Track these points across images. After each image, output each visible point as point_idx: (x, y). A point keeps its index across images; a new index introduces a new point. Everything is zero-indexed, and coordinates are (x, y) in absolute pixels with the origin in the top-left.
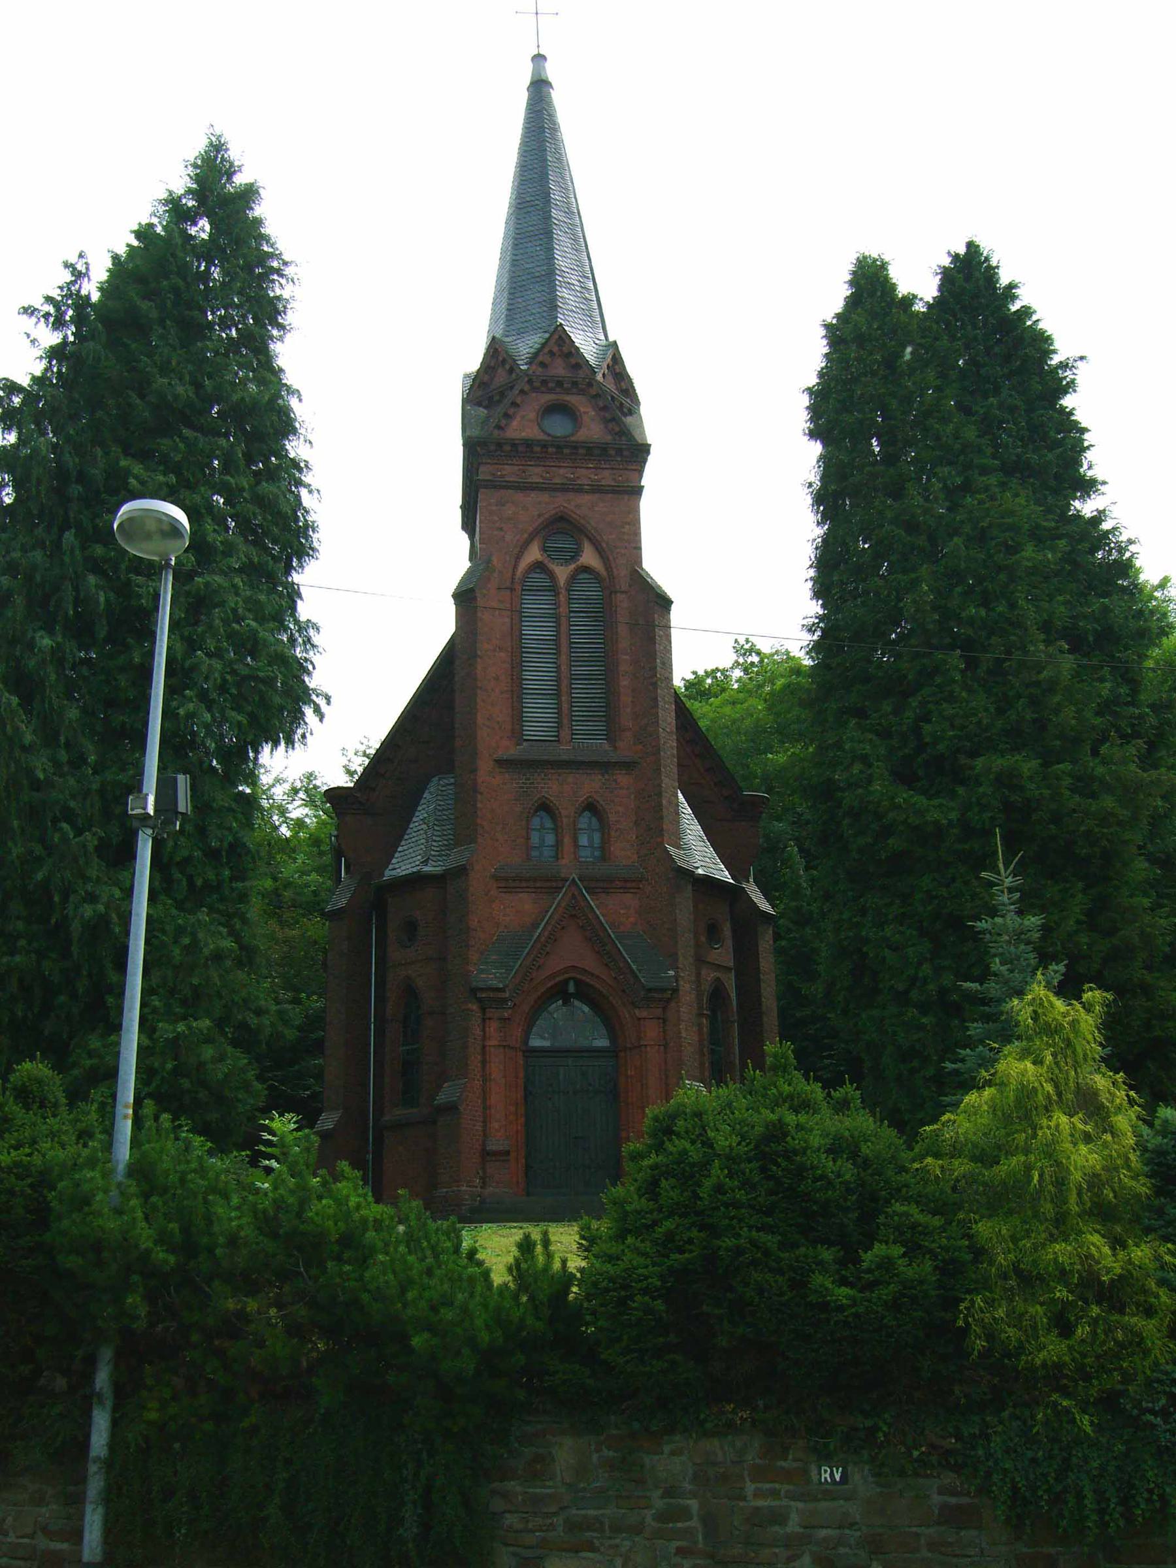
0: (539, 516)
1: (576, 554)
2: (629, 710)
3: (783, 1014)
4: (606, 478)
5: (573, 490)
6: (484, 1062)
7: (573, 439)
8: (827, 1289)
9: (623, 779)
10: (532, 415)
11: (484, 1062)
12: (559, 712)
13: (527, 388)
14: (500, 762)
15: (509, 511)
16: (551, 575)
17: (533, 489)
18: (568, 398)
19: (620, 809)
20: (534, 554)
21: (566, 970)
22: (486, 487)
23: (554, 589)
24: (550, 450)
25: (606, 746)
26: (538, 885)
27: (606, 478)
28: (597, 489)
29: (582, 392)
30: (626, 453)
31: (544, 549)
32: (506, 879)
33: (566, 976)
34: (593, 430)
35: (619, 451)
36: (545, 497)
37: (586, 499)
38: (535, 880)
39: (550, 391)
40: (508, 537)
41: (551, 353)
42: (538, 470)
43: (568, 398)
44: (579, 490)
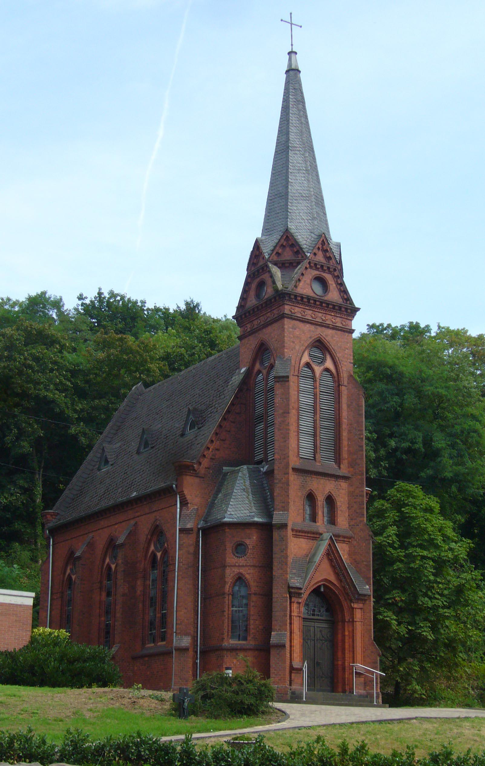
0: (310, 338)
1: (323, 361)
2: (346, 449)
3: (165, 578)
4: (338, 322)
5: (325, 327)
6: (291, 624)
7: (323, 298)
8: (163, 705)
9: (344, 484)
10: (308, 281)
11: (291, 624)
12: (315, 445)
13: (308, 266)
14: (294, 469)
15: (297, 333)
16: (313, 371)
17: (308, 323)
18: (324, 274)
19: (342, 500)
20: (306, 358)
21: (322, 581)
22: (288, 318)
23: (314, 378)
24: (324, 305)
25: (336, 466)
26: (309, 535)
27: (338, 322)
28: (335, 328)
29: (330, 272)
30: (349, 311)
31: (310, 355)
32: (296, 531)
33: (320, 584)
34: (334, 296)
35: (346, 309)
36: (312, 327)
37: (330, 332)
38: (308, 532)
39: (317, 269)
40: (297, 347)
41: (283, 246)
42: (310, 312)
43: (324, 274)
44: (327, 327)
